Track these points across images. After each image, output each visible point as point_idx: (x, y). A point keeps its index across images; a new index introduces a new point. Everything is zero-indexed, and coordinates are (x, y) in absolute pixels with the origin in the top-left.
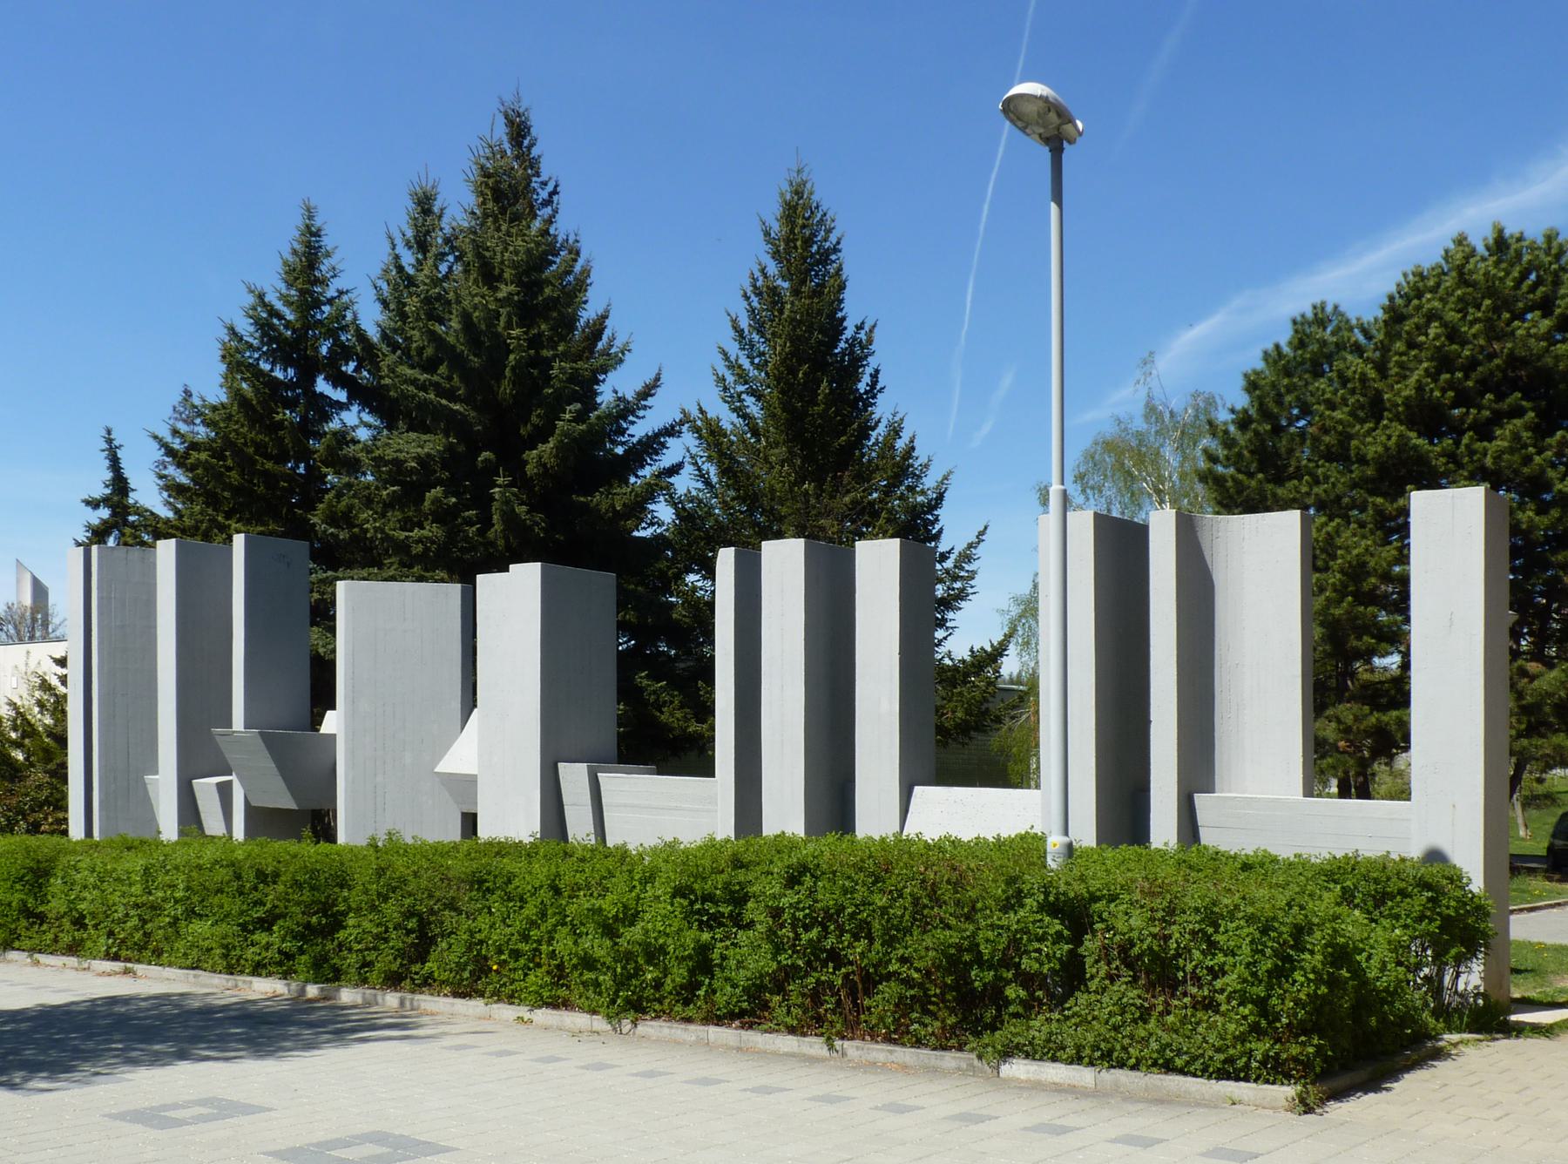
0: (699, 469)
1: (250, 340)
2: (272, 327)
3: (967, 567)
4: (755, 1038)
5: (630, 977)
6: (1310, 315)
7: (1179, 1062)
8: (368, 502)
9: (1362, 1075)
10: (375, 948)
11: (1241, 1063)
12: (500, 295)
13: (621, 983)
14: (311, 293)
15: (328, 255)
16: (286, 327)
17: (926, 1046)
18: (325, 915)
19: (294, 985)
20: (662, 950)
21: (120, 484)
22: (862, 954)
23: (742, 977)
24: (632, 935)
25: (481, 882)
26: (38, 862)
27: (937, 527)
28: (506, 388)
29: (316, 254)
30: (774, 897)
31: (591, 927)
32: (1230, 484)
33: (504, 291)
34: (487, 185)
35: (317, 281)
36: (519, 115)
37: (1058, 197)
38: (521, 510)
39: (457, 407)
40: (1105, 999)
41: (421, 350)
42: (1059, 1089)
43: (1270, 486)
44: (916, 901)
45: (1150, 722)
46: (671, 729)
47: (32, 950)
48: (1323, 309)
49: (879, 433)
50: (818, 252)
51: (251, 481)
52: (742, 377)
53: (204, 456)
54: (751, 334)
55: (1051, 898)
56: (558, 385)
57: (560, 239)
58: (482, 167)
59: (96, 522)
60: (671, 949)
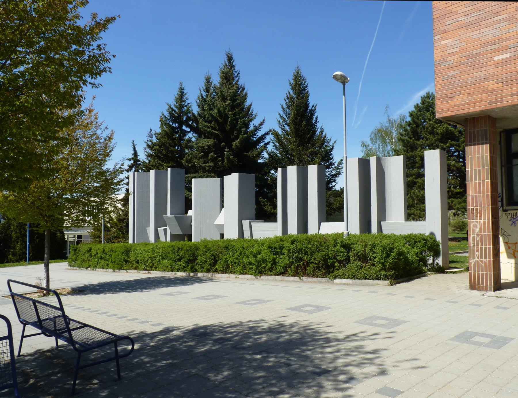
0: (274, 144)
1: (168, 117)
2: (173, 114)
3: (340, 166)
4: (285, 278)
5: (259, 266)
6: (426, 95)
7: (368, 277)
8: (196, 157)
9: (406, 279)
10: (204, 264)
11: (379, 276)
12: (227, 104)
13: (257, 268)
14: (182, 105)
15: (186, 94)
16: (176, 113)
17: (319, 277)
18: (193, 257)
19: (188, 273)
20: (266, 260)
21: (136, 154)
22: (306, 258)
23: (282, 265)
24: (259, 257)
25: (227, 247)
26: (127, 248)
27: (332, 156)
28: (228, 127)
29: (183, 94)
30: (288, 247)
31: (251, 256)
32: (405, 141)
33: (228, 102)
34: (223, 75)
35: (183, 101)
36: (230, 55)
37: (344, 94)
38: (231, 157)
39: (216, 132)
40: (354, 265)
41: (208, 118)
42: (344, 284)
43: (415, 141)
44: (317, 245)
45: (371, 205)
46: (267, 212)
47: (126, 269)
48: (429, 94)
49: (318, 133)
50: (302, 88)
51: (168, 153)
52: (284, 121)
53: (157, 147)
54: (286, 109)
55: (343, 244)
56: (240, 125)
57: (240, 86)
58: (222, 72)
59: (130, 164)
60: (268, 260)
